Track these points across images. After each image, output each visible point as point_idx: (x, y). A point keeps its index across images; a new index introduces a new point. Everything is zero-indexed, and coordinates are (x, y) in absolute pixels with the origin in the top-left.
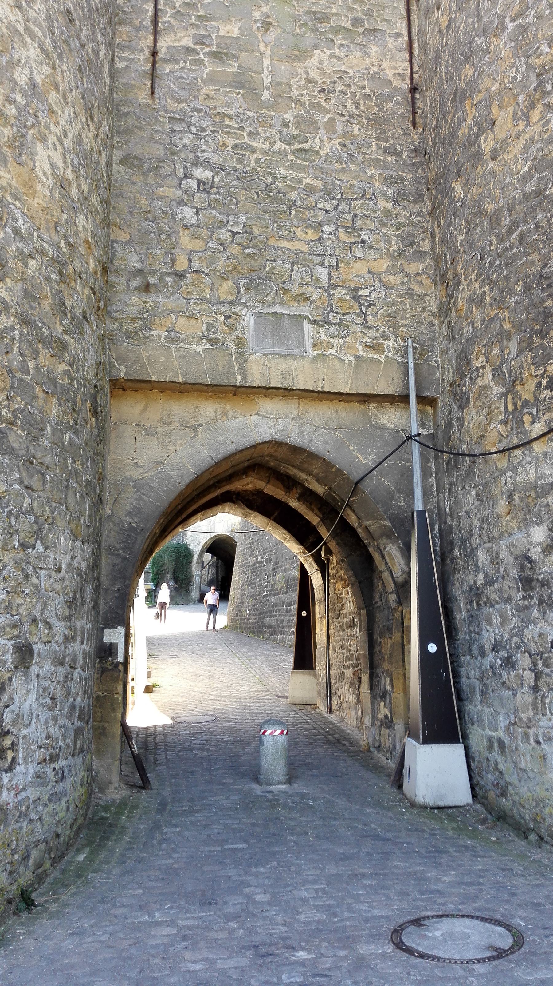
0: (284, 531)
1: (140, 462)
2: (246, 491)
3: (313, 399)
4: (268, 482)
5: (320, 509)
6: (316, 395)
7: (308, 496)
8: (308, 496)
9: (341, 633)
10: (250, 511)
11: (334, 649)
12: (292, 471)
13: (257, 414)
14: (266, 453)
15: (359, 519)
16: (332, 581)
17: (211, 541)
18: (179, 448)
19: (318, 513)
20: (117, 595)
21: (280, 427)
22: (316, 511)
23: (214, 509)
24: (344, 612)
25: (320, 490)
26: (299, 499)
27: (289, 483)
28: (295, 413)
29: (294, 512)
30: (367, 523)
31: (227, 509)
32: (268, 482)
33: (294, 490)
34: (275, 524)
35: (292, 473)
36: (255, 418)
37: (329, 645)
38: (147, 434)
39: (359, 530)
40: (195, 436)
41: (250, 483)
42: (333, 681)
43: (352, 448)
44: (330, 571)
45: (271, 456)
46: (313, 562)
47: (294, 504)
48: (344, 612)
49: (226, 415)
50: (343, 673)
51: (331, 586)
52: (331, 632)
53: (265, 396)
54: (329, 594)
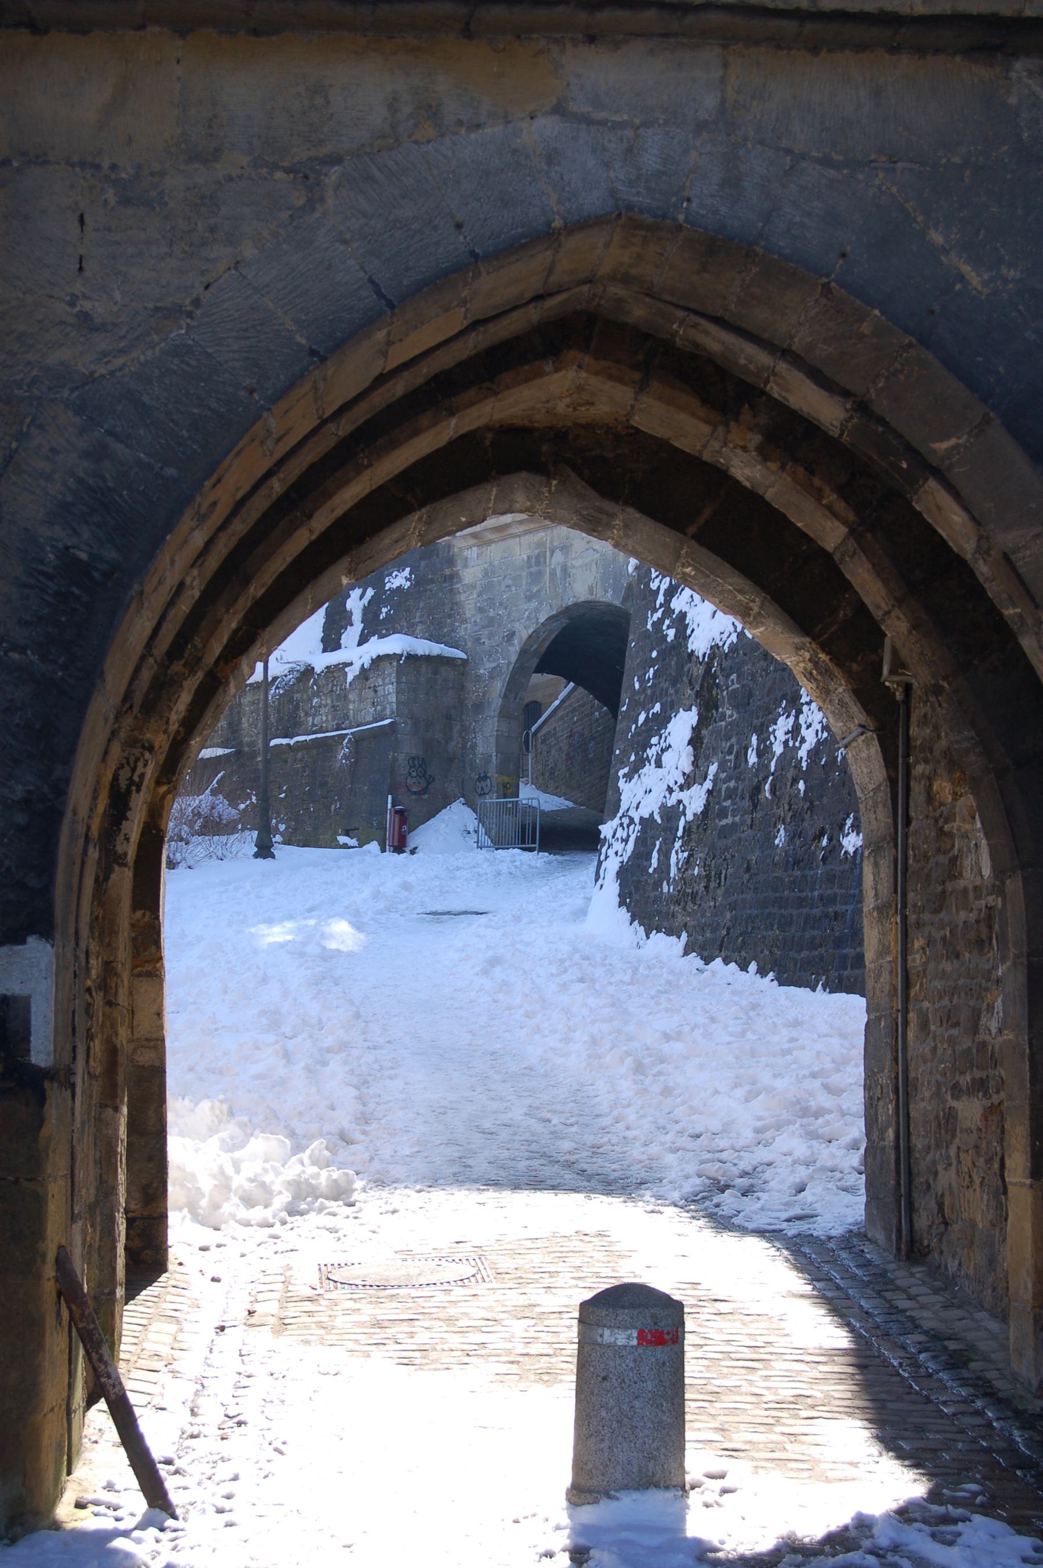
0: (738, 580)
1: (99, 309)
2: (590, 427)
3: (778, 43)
4: (642, 387)
5: (844, 491)
6: (790, 26)
7: (790, 437)
8: (790, 437)
9: (948, 966)
10: (608, 505)
11: (924, 1025)
12: (715, 341)
13: (559, 110)
14: (605, 269)
15: (977, 522)
16: (919, 769)
17: (557, 627)
18: (249, 252)
19: (840, 506)
20: (21, 819)
21: (650, 160)
22: (830, 497)
23: (469, 497)
24: (962, 883)
25: (828, 412)
26: (764, 455)
27: (723, 392)
28: (710, 101)
29: (751, 500)
30: (1008, 539)
31: (520, 498)
32: (642, 387)
33: (746, 415)
34: (702, 552)
35: (715, 347)
36: (547, 126)
37: (906, 1011)
38: (126, 201)
39: (983, 569)
40: (311, 205)
41: (558, 392)
42: (919, 1143)
43: (937, 238)
44: (914, 731)
45: (626, 279)
46: (848, 698)
47: (746, 469)
48: (962, 883)
49: (431, 111)
50: (951, 1115)
51: (917, 789)
52: (916, 960)
53: (591, 39)
54: (908, 821)
